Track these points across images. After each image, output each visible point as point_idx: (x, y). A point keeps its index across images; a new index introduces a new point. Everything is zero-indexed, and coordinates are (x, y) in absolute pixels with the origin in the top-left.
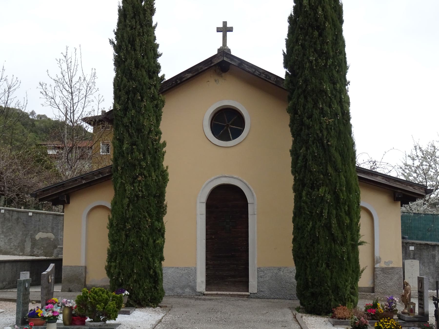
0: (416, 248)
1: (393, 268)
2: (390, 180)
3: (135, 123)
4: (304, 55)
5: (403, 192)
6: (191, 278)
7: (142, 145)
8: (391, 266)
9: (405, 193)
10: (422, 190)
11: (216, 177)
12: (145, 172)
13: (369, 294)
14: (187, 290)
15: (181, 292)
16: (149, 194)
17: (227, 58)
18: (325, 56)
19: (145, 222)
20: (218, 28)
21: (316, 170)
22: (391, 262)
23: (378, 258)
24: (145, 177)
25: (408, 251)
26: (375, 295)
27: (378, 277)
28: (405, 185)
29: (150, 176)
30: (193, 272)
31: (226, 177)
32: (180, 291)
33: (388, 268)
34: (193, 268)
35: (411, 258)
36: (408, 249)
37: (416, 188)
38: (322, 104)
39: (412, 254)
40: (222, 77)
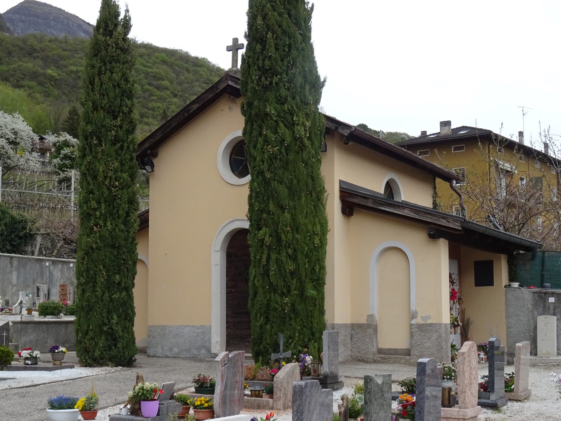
0: (557, 299)
1: (431, 325)
2: (419, 213)
3: (92, 169)
4: (249, 74)
5: (437, 227)
6: (207, 337)
7: (97, 193)
8: (429, 322)
9: (439, 228)
10: (457, 224)
11: (229, 221)
12: (101, 223)
13: (404, 358)
14: (203, 351)
15: (197, 354)
16: (104, 246)
17: (232, 81)
18: (270, 73)
19: (101, 275)
20: (228, 47)
21: (258, 209)
22: (429, 317)
23: (414, 311)
24: (101, 227)
25: (547, 305)
26: (410, 359)
27: (414, 336)
28: (437, 218)
29: (105, 225)
30: (206, 331)
31: (239, 220)
32: (195, 352)
33: (426, 324)
34: (208, 326)
35: (551, 313)
36: (547, 302)
37: (450, 220)
38: (267, 130)
39: (552, 307)
40: (236, 103)
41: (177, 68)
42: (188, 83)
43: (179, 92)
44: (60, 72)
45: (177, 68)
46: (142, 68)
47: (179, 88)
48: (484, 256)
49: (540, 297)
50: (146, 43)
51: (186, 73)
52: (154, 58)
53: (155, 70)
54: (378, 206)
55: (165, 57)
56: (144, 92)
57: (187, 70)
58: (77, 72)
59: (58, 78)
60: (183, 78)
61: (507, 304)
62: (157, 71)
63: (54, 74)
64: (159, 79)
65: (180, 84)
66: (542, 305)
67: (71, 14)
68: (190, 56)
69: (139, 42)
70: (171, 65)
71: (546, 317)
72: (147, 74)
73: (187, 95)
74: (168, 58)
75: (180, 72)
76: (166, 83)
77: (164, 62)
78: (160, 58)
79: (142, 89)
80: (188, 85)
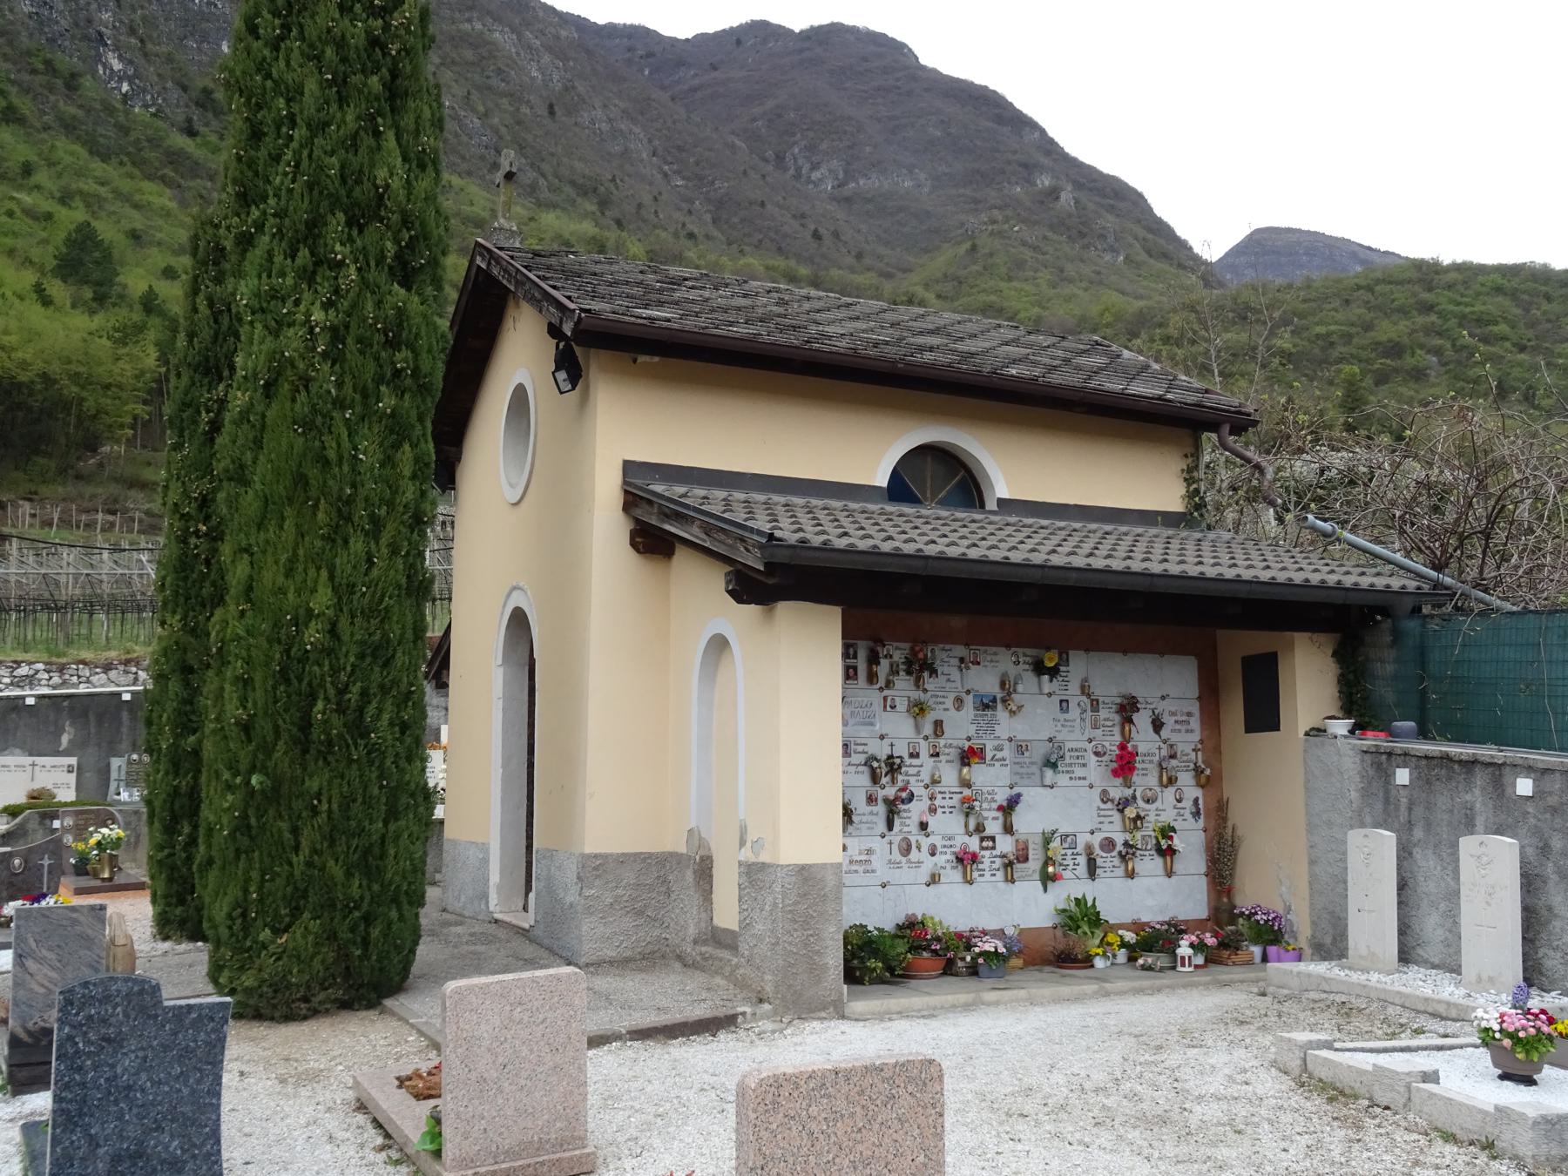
41: (1525, 297)
42: (1549, 321)
43: (1529, 340)
44: (1298, 341)
45: (1525, 297)
46: (1451, 307)
47: (1530, 333)
48: (1257, 642)
49: (1378, 766)
50: (1459, 261)
51: (1545, 303)
52: (1477, 287)
53: (1478, 308)
54: (663, 522)
55: (1500, 281)
56: (1456, 352)
57: (1548, 298)
58: (1329, 334)
59: (1293, 350)
60: (1539, 313)
61: (1309, 789)
62: (1482, 308)
63: (1286, 345)
64: (1489, 323)
65: (1532, 325)
66: (1381, 794)
67: (1336, 238)
68: (1553, 270)
69: (1445, 263)
70: (1513, 295)
71: (1366, 836)
72: (1464, 317)
73: (1547, 345)
74: (1505, 282)
75: (1531, 303)
76: (1503, 328)
77: (1499, 290)
78: (1489, 284)
79: (1454, 346)
80: (1549, 326)
